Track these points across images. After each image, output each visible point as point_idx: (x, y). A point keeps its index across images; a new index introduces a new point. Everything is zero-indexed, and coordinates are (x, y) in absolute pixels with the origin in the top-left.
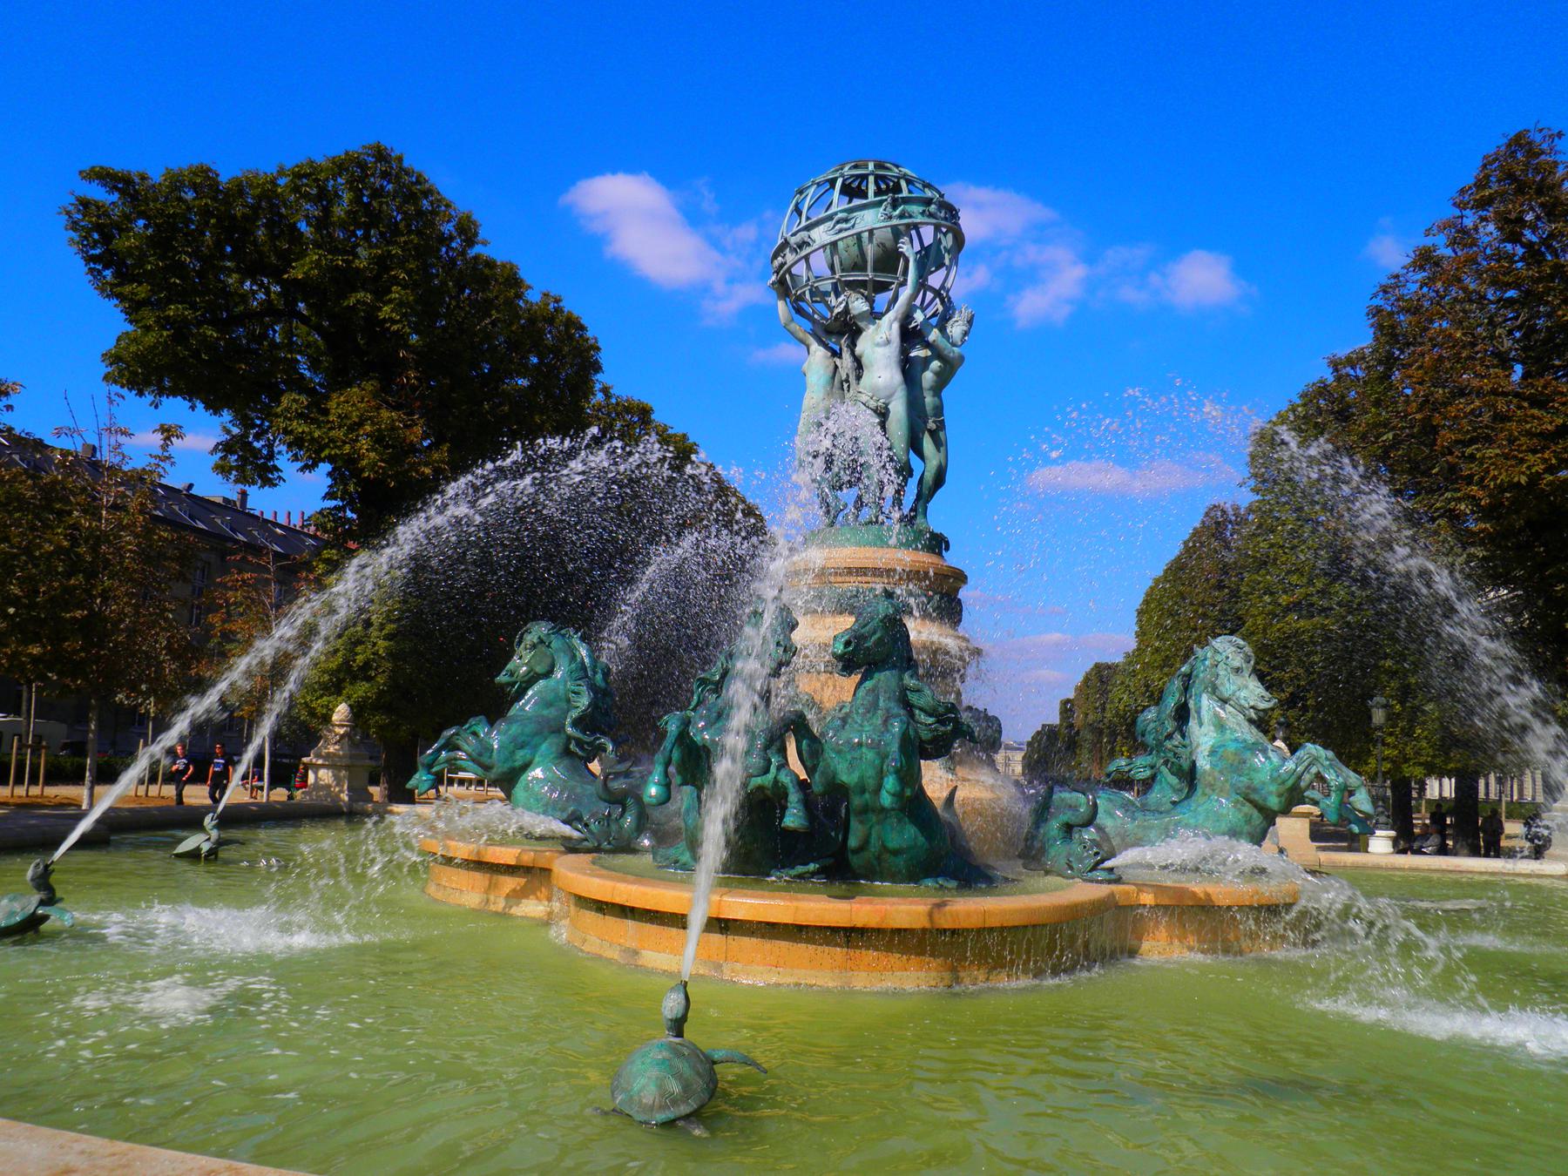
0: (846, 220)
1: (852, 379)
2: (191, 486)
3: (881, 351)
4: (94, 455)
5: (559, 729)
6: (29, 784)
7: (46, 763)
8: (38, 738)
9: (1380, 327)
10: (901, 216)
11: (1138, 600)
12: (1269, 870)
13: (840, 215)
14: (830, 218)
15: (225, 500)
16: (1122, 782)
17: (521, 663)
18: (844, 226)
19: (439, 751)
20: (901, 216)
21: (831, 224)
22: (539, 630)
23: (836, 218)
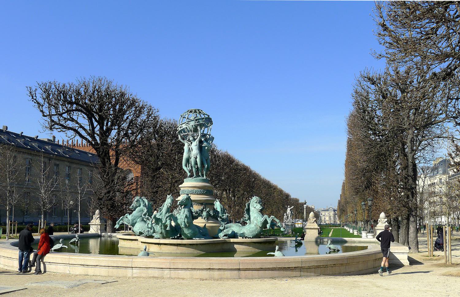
0: (188, 123)
2: (37, 137)
3: (195, 147)
4: (7, 129)
5: (142, 216)
6: (17, 233)
7: (17, 228)
8: (334, 242)
9: (357, 103)
10: (198, 122)
11: (344, 162)
12: (142, 231)
13: (187, 123)
14: (185, 123)
15: (48, 140)
16: (123, 227)
17: (134, 204)
18: (188, 124)
19: (120, 221)
20: (198, 122)
21: (185, 124)
22: (137, 198)
23: (186, 123)
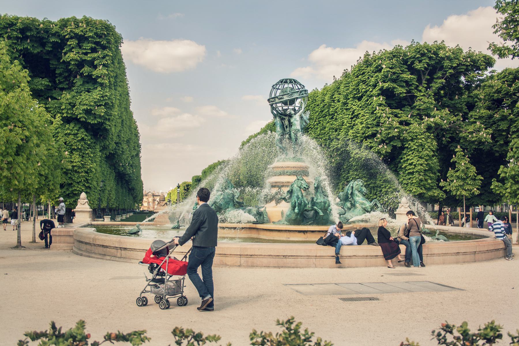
0: (291, 95)
1: (288, 126)
